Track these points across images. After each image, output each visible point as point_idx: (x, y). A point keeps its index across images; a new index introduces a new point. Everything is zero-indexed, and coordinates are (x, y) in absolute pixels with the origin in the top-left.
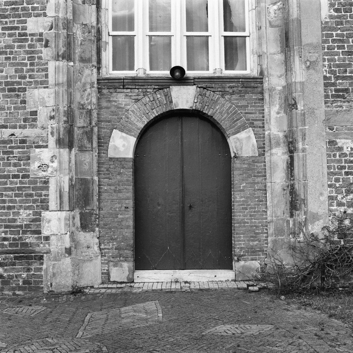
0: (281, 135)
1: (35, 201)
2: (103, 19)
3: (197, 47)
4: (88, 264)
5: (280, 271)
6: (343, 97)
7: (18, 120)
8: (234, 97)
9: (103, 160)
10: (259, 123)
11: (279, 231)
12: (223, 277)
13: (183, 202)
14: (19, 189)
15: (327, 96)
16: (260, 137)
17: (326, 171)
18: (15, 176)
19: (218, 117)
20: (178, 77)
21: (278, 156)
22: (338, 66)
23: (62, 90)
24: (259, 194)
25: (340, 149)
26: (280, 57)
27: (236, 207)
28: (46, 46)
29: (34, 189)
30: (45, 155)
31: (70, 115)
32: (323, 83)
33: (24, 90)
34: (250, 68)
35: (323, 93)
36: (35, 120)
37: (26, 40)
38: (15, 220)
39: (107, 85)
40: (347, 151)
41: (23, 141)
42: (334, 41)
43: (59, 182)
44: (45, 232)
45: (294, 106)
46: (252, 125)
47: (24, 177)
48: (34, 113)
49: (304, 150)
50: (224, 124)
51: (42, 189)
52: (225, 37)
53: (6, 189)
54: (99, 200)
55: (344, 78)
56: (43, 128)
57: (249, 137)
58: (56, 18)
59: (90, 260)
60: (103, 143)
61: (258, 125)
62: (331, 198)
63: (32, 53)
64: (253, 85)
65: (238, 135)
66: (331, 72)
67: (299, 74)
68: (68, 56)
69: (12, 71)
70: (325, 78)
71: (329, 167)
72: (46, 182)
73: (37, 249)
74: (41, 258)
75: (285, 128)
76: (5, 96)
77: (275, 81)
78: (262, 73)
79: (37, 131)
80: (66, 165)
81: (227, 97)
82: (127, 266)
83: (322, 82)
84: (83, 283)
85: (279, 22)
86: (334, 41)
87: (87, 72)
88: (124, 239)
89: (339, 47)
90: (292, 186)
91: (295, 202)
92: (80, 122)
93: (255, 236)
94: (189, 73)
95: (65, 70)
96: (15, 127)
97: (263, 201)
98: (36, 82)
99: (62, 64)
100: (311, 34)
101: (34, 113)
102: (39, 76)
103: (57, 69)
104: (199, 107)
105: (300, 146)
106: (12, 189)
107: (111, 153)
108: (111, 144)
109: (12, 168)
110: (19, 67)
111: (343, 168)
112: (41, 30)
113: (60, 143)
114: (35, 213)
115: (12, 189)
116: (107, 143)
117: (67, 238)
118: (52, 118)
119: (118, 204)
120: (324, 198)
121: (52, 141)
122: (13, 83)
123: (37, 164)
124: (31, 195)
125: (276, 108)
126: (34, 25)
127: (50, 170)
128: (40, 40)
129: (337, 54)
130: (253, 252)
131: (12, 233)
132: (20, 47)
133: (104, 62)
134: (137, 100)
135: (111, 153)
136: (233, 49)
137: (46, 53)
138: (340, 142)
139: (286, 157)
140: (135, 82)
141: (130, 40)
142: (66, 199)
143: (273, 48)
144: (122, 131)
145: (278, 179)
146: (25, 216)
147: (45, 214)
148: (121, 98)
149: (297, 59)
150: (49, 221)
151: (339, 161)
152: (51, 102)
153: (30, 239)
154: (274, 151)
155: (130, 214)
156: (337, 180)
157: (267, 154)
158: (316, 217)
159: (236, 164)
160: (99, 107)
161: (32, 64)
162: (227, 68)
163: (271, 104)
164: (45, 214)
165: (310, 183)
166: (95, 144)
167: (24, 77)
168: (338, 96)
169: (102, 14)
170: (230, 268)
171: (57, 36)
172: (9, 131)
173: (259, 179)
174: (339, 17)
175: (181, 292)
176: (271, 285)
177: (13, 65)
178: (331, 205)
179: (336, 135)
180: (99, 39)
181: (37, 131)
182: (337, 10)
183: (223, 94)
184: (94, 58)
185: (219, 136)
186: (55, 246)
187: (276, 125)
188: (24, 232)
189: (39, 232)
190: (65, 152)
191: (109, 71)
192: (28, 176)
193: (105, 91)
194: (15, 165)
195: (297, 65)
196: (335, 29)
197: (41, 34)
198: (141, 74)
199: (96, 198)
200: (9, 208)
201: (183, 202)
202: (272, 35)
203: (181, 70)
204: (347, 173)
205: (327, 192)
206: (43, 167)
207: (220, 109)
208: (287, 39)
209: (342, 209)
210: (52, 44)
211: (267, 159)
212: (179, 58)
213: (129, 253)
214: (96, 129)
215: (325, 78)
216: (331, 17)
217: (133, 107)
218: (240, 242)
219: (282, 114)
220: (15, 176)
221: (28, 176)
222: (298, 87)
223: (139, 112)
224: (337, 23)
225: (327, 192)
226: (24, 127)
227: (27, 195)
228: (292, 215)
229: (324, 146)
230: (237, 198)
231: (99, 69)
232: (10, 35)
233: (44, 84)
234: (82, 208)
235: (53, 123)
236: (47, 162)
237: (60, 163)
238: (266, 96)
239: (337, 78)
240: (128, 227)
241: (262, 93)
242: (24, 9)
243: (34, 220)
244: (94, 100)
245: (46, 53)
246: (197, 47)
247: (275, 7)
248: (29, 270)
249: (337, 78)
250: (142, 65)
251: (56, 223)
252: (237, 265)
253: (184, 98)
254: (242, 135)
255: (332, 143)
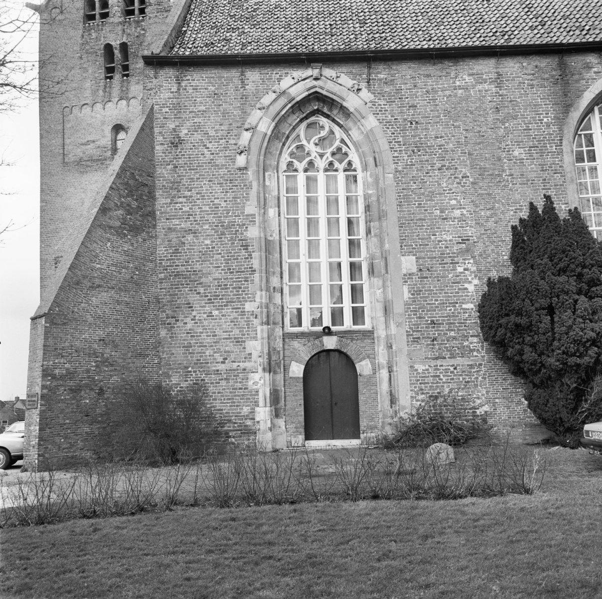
0: (385, 362)
1: (251, 402)
2: (284, 300)
3: (337, 316)
4: (280, 436)
5: (385, 438)
6: (417, 342)
7: (242, 358)
8: (358, 342)
9: (287, 378)
10: (372, 356)
11: (385, 416)
12: (355, 443)
13: (331, 401)
14: (243, 395)
15: (408, 342)
16: (373, 364)
17: (409, 382)
18: (240, 389)
19: (313, 246)
20: (327, 332)
21: (384, 373)
22: (414, 325)
23: (266, 341)
24: (373, 395)
25: (416, 370)
26: (383, 319)
27: (361, 403)
28: (256, 318)
29: (250, 395)
30: (256, 377)
31: (269, 354)
32: (595, 145)
33: (245, 342)
34: (367, 326)
35: (406, 340)
36: (250, 358)
37: (245, 315)
38: (240, 413)
39: (287, 336)
40: (420, 371)
41: (244, 370)
42: (411, 311)
43: (264, 392)
44: (257, 419)
45: (391, 347)
46: (368, 357)
47: (245, 389)
48: (250, 354)
49: (397, 371)
50: (353, 357)
51: (255, 395)
52: (353, 307)
53: (235, 396)
54: (285, 401)
55: (417, 331)
56: (255, 362)
57: (367, 364)
58: (261, 303)
59: (281, 434)
60: (286, 369)
61: (372, 357)
62: (412, 397)
63: (248, 322)
64: (369, 334)
65: (361, 363)
66: (410, 328)
67: (393, 329)
68: (268, 323)
69: (237, 331)
70: (407, 331)
71: (410, 380)
72: (257, 392)
73: (254, 428)
74: (255, 433)
75: (387, 359)
76: (234, 345)
77: (381, 332)
78: (373, 328)
79: (252, 364)
80: (268, 382)
81: (354, 342)
82: (301, 437)
83: (405, 334)
84: (278, 447)
85: (382, 300)
86: (411, 311)
87: (277, 330)
88: (299, 422)
89: (414, 315)
90: (391, 391)
91: (393, 401)
92: (274, 358)
93: (372, 419)
94: (334, 329)
95: (266, 331)
96: (240, 362)
97: (375, 399)
98: (251, 338)
99: (265, 327)
100: (398, 308)
101: (250, 354)
102: (252, 334)
103: (262, 330)
104: (339, 348)
105: (395, 369)
106: (239, 396)
107: (291, 375)
108: (291, 369)
109: (239, 384)
110: (241, 329)
111: (419, 380)
112: (253, 309)
113: (264, 370)
114: (252, 409)
115: (239, 396)
116: (289, 369)
117: (269, 422)
118: (260, 356)
119: (295, 402)
120: (409, 397)
121: (260, 369)
122: (238, 338)
123: (252, 382)
124: (249, 399)
125: (382, 347)
126: (249, 307)
127: (259, 385)
128: (253, 315)
129: (413, 318)
130: (372, 428)
131: (239, 419)
132: (241, 318)
133: (285, 323)
134: (304, 345)
135: (291, 375)
136: (358, 315)
137: (256, 322)
138: (416, 366)
139: (388, 375)
140: (303, 335)
141: (341, 309)
142: (268, 400)
143: (380, 314)
144: (297, 362)
145: (385, 387)
146: (246, 410)
147: (257, 409)
148: (296, 344)
149: (392, 321)
150: (259, 413)
151: (417, 377)
152: (259, 348)
153: (249, 423)
154: (381, 371)
155: (302, 408)
156: (415, 387)
157: (377, 373)
158: (404, 408)
159: (360, 379)
160: (284, 349)
161: (248, 328)
162: (354, 324)
163: (378, 346)
164: (257, 409)
165: (401, 389)
166: (282, 370)
167: (244, 335)
168: (414, 341)
169: (284, 297)
170: (359, 438)
171: (262, 312)
172: (237, 364)
173: (373, 388)
174: (414, 298)
175: (332, 450)
176: (381, 446)
177: (237, 328)
178: (412, 401)
179: (414, 363)
180: (283, 311)
181: (252, 364)
182: (412, 294)
183: (352, 340)
184: (281, 322)
185: (349, 363)
186: (262, 426)
187: (382, 357)
188: (246, 419)
189: (254, 419)
190: (267, 375)
191: (289, 329)
192: (247, 388)
193: (287, 340)
194: (240, 382)
195: (393, 326)
196: (412, 305)
197: (253, 312)
198: (306, 330)
199: (283, 400)
200: (237, 406)
201: (331, 401)
202: (380, 307)
203: (328, 328)
204: (420, 383)
205: (410, 394)
206: (255, 383)
207: (351, 349)
208: (387, 310)
209: (419, 403)
210: (259, 317)
211: (378, 376)
212: (327, 322)
213: (302, 430)
214: (282, 362)
215: (407, 331)
216: (409, 298)
217: (302, 348)
218: (363, 423)
219: (385, 351)
220: (240, 389)
221: (247, 388)
222: (393, 337)
223: (304, 351)
224: (413, 301)
225: (410, 394)
226: (245, 362)
227: (247, 399)
228: (391, 407)
229: (407, 368)
230: (361, 398)
231: (283, 328)
232: (236, 312)
233: (255, 338)
234: (276, 405)
235: (261, 360)
236: (258, 380)
237: (264, 380)
238: (376, 341)
239: (414, 331)
240: (301, 416)
241: (373, 339)
242: (243, 298)
243: (251, 413)
244: (281, 346)
245: (256, 322)
246: (337, 316)
247: (380, 291)
248: (249, 440)
249: (414, 331)
250: (306, 326)
251: (263, 413)
252: (362, 436)
253: (330, 343)
254: (363, 363)
255: (411, 367)
